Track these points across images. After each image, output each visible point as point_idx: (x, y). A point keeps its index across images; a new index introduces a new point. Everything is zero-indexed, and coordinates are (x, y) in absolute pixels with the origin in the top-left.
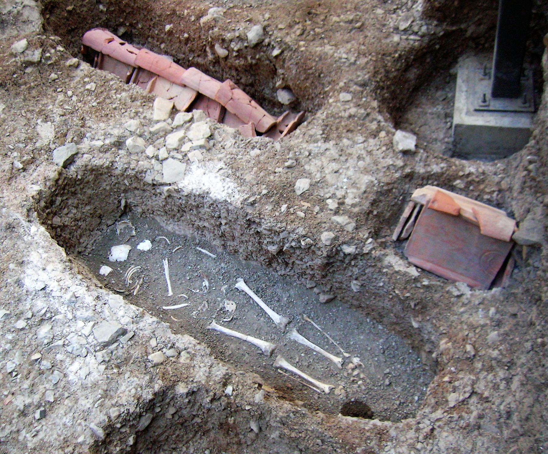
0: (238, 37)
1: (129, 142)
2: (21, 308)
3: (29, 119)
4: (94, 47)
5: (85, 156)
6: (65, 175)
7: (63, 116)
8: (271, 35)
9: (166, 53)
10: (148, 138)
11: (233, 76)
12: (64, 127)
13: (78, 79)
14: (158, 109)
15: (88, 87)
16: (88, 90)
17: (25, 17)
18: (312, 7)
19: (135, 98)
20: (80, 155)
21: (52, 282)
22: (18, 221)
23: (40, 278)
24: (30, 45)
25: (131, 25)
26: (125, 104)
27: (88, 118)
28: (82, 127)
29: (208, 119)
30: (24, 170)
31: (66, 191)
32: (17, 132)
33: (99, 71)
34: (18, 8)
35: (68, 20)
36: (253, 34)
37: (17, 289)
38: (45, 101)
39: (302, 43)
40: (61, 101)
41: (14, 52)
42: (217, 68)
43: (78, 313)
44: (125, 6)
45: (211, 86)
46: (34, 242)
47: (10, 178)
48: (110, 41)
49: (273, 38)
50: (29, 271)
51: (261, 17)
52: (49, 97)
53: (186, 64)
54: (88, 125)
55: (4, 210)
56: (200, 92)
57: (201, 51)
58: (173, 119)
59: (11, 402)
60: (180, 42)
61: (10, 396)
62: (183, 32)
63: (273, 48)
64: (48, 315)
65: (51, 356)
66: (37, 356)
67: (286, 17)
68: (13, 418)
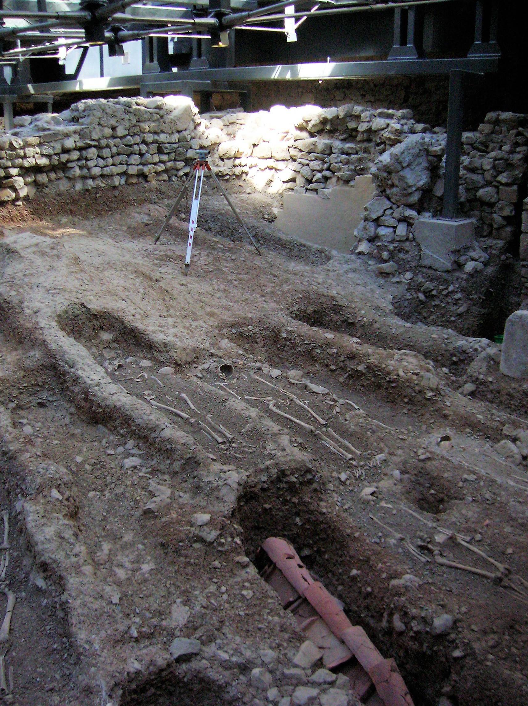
0: (422, 618)
1: (256, 671)
3: (169, 593)
4: (271, 555)
5: (204, 661)
6: (172, 669)
7: (204, 608)
8: (460, 632)
9: (340, 597)
10: (278, 677)
11: (399, 657)
12: (200, 620)
13: (238, 579)
14: (303, 653)
15: (245, 592)
16: (243, 595)
17: (220, 494)
18: (517, 622)
19: (286, 629)
20: (199, 658)
22: (100, 689)
24: (211, 522)
25: (318, 551)
26: (272, 630)
27: (227, 624)
28: (217, 629)
29: (351, 692)
30: (137, 640)
31: (164, 686)
32: (151, 599)
33: (263, 582)
34: (219, 482)
35: (260, 516)
36: (441, 621)
38: (195, 583)
39: (491, 657)
40: (211, 593)
41: (193, 521)
42: (386, 639)
44: (321, 530)
45: (371, 656)
48: (290, 557)
49: (460, 636)
51: (456, 607)
52: (202, 582)
53: (356, 620)
54: (224, 631)
55: (93, 669)
56: (357, 657)
57: (377, 612)
58: (313, 672)
60: (360, 593)
62: (368, 584)
63: (457, 647)
67: (485, 620)
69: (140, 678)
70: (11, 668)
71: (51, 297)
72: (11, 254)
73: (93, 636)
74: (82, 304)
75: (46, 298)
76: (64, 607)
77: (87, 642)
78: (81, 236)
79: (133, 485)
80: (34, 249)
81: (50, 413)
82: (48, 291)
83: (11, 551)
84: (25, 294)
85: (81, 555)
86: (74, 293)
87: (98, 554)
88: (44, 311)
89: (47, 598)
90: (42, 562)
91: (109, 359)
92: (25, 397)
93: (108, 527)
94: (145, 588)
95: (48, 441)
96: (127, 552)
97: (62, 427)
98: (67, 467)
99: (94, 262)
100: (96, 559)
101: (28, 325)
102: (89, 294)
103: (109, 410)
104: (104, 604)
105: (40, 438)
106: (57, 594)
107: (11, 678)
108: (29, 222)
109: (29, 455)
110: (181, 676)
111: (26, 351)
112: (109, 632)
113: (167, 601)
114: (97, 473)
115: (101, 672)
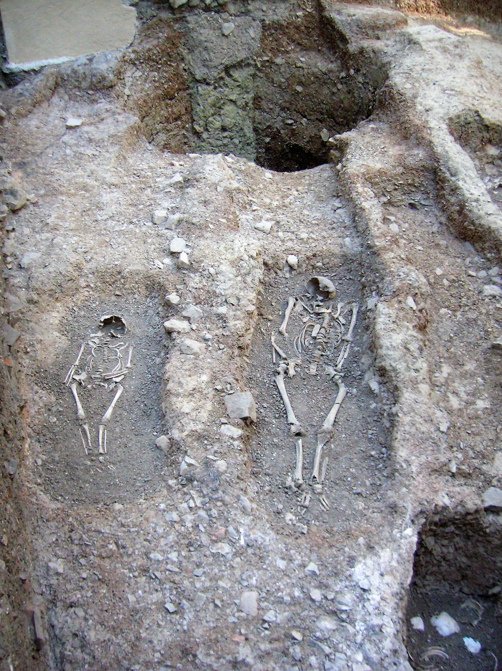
2: (330, 582)
6: (478, 516)
21: (376, 593)
23: (372, 579)
30: (453, 475)
32: (478, 438)
37: (345, 563)
43: (367, 646)
46: (398, 543)
47: (436, 470)
50: (369, 562)
55: (404, 490)
59: (238, 643)
61: (243, 638)
64: (344, 616)
65: (308, 650)
66: (298, 636)
68: (224, 658)
69: (445, 514)
70: (327, 459)
71: (446, 98)
72: (412, 45)
73: (413, 458)
74: (477, 112)
75: (441, 98)
76: (392, 417)
77: (406, 461)
78: (484, 39)
79: (487, 314)
80: (437, 44)
81: (420, 217)
82: (444, 91)
83: (353, 345)
84: (420, 90)
85: (422, 371)
86: (470, 99)
87: (437, 375)
88: (436, 111)
89: (377, 403)
90: (382, 366)
91: (490, 176)
92: (399, 194)
93: (452, 350)
94: (474, 425)
95: (412, 244)
96: (466, 382)
97: (429, 234)
98: (426, 277)
99: (495, 70)
100: (434, 379)
101: (418, 122)
102: (485, 102)
103: (481, 230)
104: (432, 429)
105: (405, 239)
106: (388, 402)
107: (324, 469)
108: (433, 15)
109: (392, 255)
110: (485, 525)
111: (409, 148)
112: (430, 459)
113: (494, 446)
114: (454, 291)
115: (411, 495)
